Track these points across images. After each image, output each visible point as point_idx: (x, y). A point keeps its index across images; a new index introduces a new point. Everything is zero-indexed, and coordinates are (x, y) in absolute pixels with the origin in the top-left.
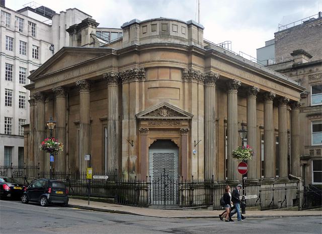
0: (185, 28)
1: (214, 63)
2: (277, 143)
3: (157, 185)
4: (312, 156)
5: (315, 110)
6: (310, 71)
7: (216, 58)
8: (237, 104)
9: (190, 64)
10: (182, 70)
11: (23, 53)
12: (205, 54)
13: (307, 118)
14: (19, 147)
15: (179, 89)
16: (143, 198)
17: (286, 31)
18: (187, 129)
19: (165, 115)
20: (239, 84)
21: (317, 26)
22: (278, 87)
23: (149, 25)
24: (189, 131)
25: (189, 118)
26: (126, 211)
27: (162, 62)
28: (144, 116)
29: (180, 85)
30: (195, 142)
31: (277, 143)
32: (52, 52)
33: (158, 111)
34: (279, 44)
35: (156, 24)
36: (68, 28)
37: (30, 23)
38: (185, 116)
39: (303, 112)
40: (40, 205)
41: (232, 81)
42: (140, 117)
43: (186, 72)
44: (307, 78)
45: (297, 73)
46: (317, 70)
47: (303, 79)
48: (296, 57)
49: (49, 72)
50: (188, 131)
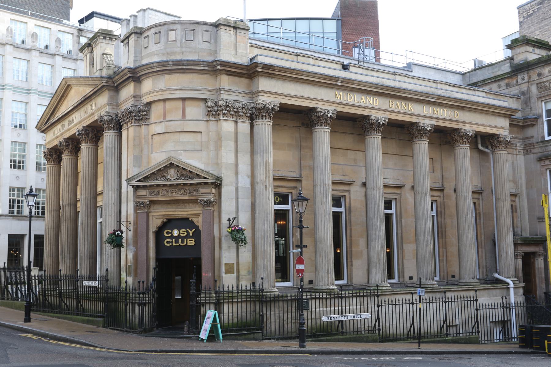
1: (264, 84)
6: (539, 75)
7: (271, 76)
8: (381, 152)
12: (248, 70)
13: (538, 165)
14: (9, 235)
16: (310, 321)
23: (151, 33)
24: (218, 201)
27: (168, 92)
28: (139, 181)
33: (161, 172)
38: (205, 178)
39: (531, 153)
40: (480, 344)
44: (534, 89)
45: (517, 82)
47: (529, 90)
48: (518, 50)
49: (59, 115)
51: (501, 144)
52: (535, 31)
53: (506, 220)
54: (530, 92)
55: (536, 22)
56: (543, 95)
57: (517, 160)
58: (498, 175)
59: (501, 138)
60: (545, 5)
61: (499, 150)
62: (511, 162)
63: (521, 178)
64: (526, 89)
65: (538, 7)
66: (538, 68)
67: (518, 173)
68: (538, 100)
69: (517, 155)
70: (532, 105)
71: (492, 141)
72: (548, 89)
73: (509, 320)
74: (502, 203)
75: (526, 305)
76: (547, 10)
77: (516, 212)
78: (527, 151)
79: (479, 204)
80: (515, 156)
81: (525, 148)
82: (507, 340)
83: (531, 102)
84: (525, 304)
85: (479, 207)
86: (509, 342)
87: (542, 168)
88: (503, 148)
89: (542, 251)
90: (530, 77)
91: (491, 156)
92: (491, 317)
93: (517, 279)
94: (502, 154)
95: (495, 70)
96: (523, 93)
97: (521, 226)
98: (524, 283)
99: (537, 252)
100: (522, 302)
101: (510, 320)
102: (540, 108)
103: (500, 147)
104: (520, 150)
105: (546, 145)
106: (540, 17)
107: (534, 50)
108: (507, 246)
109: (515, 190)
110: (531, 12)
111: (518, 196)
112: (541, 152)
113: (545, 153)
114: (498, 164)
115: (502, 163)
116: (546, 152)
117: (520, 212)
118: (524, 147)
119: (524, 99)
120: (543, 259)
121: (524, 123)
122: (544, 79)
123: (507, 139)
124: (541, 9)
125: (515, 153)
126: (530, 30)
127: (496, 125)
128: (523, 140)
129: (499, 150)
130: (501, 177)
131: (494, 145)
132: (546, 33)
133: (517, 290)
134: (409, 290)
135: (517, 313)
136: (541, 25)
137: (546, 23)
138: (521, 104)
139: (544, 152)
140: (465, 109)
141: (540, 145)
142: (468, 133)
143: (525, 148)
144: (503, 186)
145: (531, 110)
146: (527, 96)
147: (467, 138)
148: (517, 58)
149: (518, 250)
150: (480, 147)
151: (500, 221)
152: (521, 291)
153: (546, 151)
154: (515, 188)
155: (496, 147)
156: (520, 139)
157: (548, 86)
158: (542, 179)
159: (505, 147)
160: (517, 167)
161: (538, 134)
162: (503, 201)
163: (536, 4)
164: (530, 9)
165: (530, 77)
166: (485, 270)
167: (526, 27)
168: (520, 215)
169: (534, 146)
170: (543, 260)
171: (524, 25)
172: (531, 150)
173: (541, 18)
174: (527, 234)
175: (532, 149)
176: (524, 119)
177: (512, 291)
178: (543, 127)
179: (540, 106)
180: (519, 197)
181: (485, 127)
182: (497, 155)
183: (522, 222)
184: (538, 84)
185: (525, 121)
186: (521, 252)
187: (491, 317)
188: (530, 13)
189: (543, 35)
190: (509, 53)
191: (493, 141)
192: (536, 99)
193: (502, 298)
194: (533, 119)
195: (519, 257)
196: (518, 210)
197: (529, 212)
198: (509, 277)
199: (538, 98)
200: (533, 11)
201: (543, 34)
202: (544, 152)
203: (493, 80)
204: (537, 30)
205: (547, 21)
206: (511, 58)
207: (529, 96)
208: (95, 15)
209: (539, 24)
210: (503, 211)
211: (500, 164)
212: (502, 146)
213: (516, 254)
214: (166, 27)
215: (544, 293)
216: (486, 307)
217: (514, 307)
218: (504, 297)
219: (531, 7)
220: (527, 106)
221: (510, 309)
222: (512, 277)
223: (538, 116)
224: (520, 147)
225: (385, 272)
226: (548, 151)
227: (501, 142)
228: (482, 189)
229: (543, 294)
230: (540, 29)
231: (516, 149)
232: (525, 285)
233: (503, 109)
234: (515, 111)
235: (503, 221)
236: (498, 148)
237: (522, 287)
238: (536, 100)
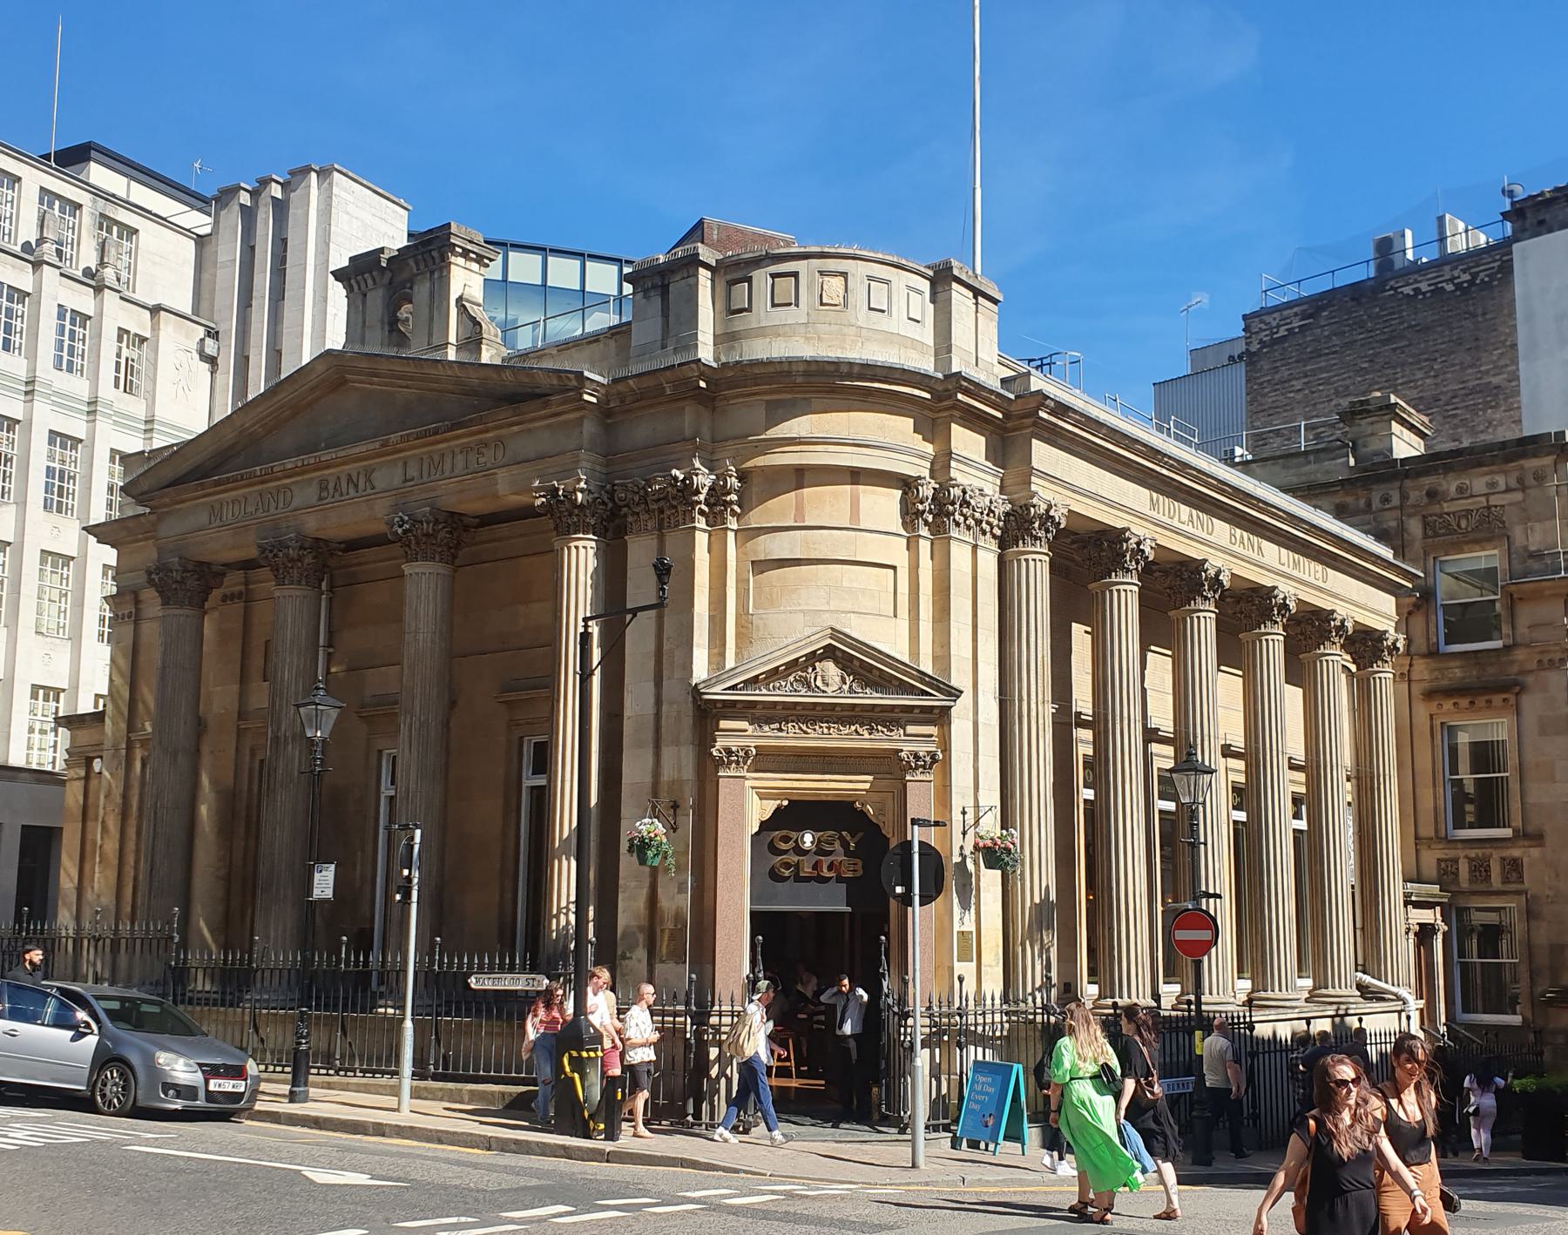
0: (920, 292)
1: (1043, 454)
2: (1241, 816)
3: (989, 1020)
7: (1055, 437)
9: (942, 463)
10: (907, 484)
11: (70, 363)
14: (23, 826)
15: (894, 568)
18: (933, 756)
19: (831, 681)
20: (1147, 550)
21: (1438, 291)
22: (1312, 570)
25: (938, 700)
28: (733, 687)
29: (896, 552)
30: (964, 813)
31: (1241, 816)
32: (207, 366)
34: (1265, 365)
36: (340, 261)
37: (105, 222)
41: (1118, 535)
42: (717, 692)
43: (927, 491)
45: (1369, 504)
50: (934, 760)
52: (1290, 380)
54: (1405, 535)
55: (1294, 359)
64: (1393, 524)
76: (1326, 333)
90: (1404, 497)
94: (1039, 563)
106: (1306, 348)
110: (1282, 332)
126: (1277, 377)
132: (1321, 388)
134: (1321, 1008)
136: (1308, 368)
137: (1323, 364)
164: (1278, 326)
165: (1404, 497)
167: (1266, 367)
171: (1262, 363)
173: (1309, 350)
189: (1313, 392)
200: (1287, 330)
201: (1314, 390)
204: (1296, 379)
205: (1325, 361)
208: (93, 154)
209: (1305, 366)
214: (816, 263)
225: (129, 909)
230: (1306, 376)
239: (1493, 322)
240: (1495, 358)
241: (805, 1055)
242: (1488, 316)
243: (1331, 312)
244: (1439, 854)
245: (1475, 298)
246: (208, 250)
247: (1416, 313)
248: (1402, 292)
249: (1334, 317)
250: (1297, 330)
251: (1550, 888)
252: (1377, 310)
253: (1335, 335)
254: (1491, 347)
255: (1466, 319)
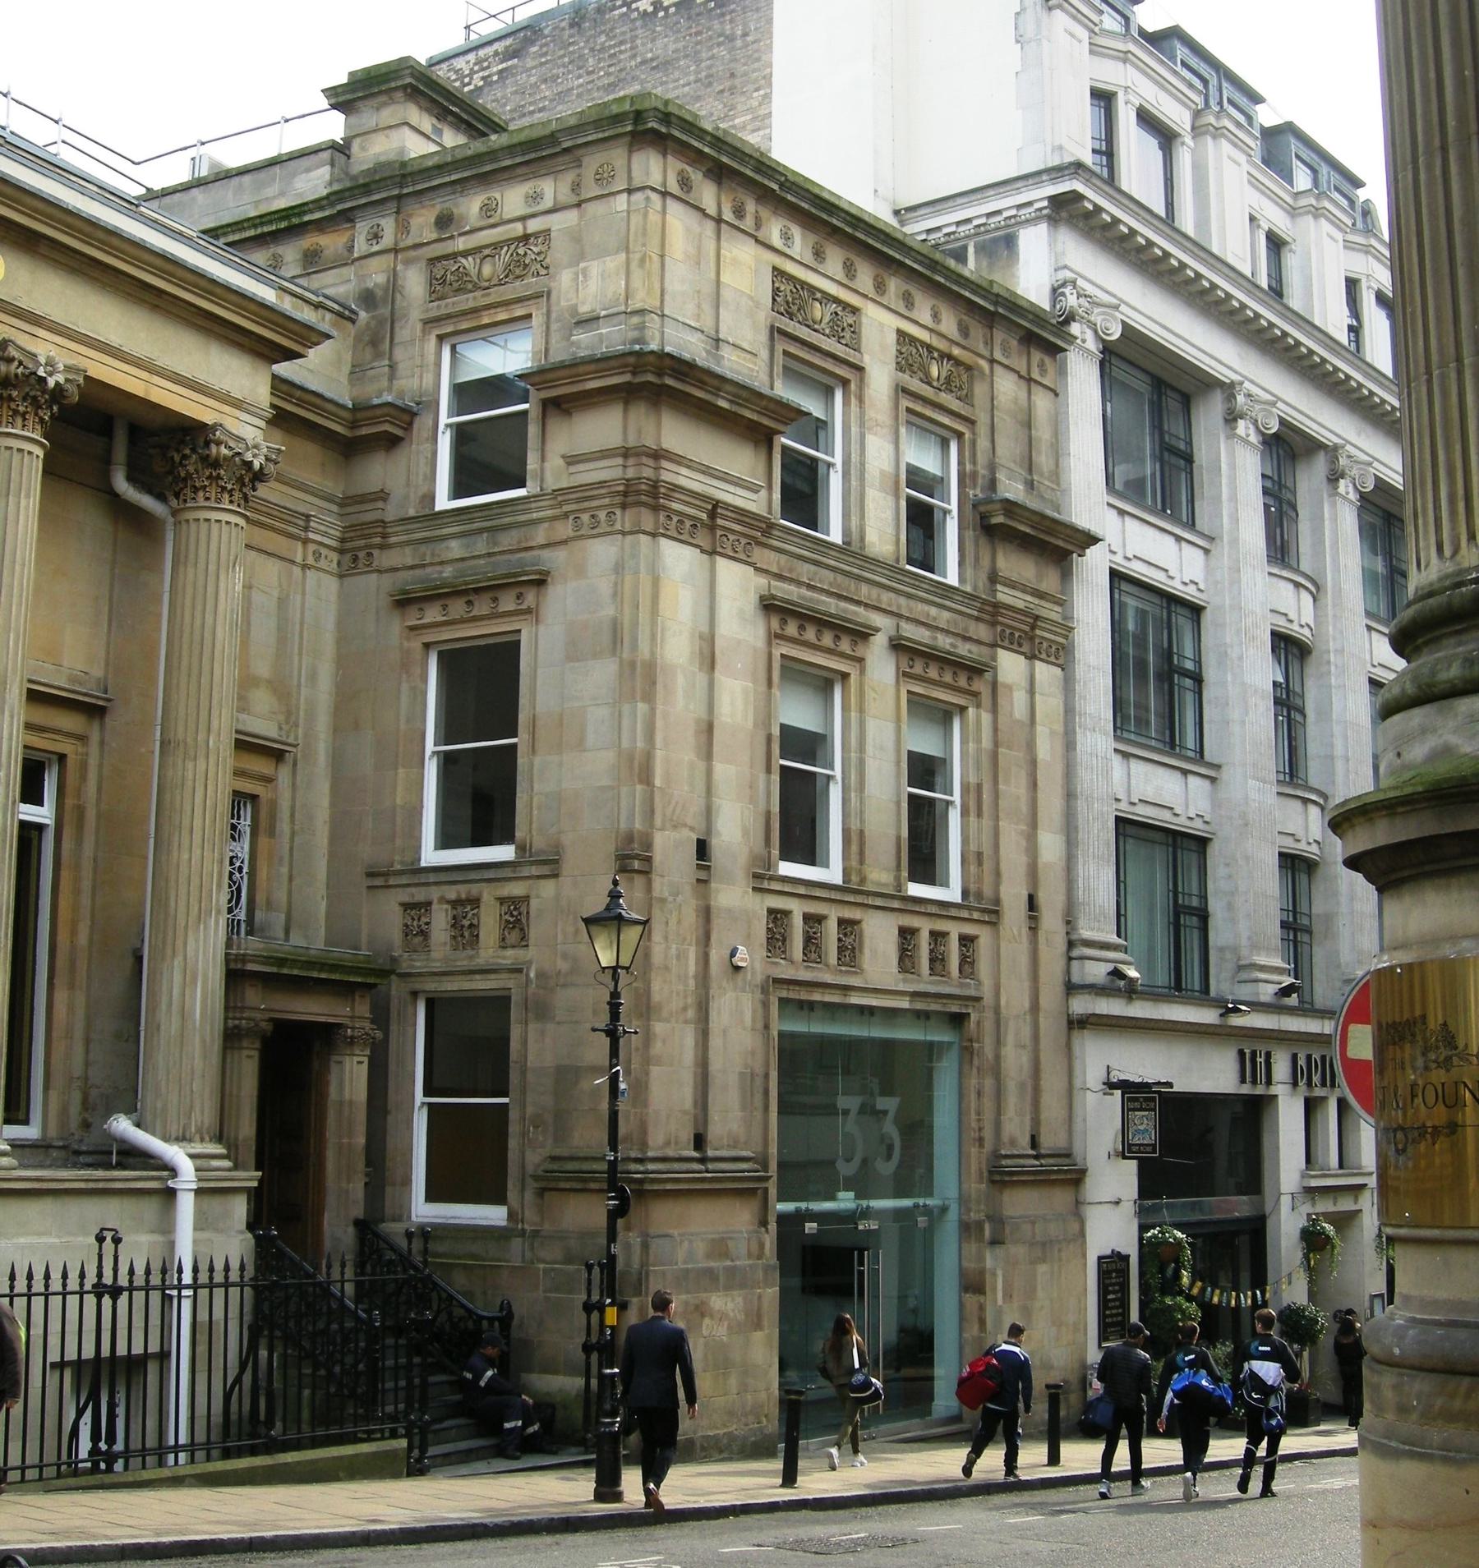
4: (419, 965)
5: (455, 548)
13: (396, 626)
17: (499, 46)
26: (61, 895)
35: (529, 316)
44: (414, 283)
46: (488, 209)
47: (393, 286)
48: (368, 118)
51: (219, 477)
53: (197, 852)
54: (398, 296)
56: (450, 310)
57: (304, 594)
58: (187, 629)
59: (218, 443)
60: (530, 63)
61: (207, 504)
62: (276, 593)
63: (313, 677)
65: (504, 65)
66: (441, 192)
67: (300, 654)
68: (423, 331)
69: (305, 567)
70: (399, 354)
71: (177, 458)
72: (470, 286)
73: (154, 1355)
74: (190, 765)
75: (356, 1274)
76: (533, 79)
77: (272, 832)
78: (355, 559)
79: (84, 766)
80: (297, 571)
81: (348, 545)
82: (103, 1466)
83: (396, 340)
84: (250, 1272)
85: (83, 777)
86: (108, 1479)
87: (408, 639)
88: (226, 496)
89: (367, 1025)
91: (170, 536)
92: (54, 1341)
93: (224, 1151)
94: (215, 527)
95: (270, 192)
96: (368, 298)
97: (289, 903)
98: (257, 1169)
99: (339, 1026)
100: (235, 1265)
101: (163, 1356)
102: (432, 367)
103: (213, 492)
104: (324, 551)
105: (438, 533)
106: (505, 105)
107: (439, 132)
108: (189, 979)
109: (280, 729)
111: (289, 758)
112: (412, 567)
113: (429, 570)
114: (191, 571)
115: (212, 568)
116: (432, 564)
117: (293, 834)
118: (343, 540)
119: (368, 323)
120: (366, 1060)
121: (354, 425)
122: (462, 239)
123: (248, 457)
124: (513, 75)
125: (299, 559)
127: (202, 376)
128: (341, 505)
129: (207, 504)
130: (197, 638)
131: (185, 480)
133: (215, 1204)
135: (203, 1316)
138: (355, 346)
139: (424, 566)
140: (43, 250)
141: (412, 531)
142: (41, 372)
143: (348, 545)
144: (205, 680)
145: (392, 377)
146: (385, 311)
147: (35, 398)
148: (363, 149)
149: (243, 1008)
150: (122, 485)
151: (169, 852)
152: (240, 1208)
153: (437, 560)
154: (282, 718)
155: (196, 490)
156: (329, 498)
157: (473, 272)
158: (405, 687)
159: (237, 495)
160: (302, 624)
161: (408, 485)
162: (195, 759)
163: (496, 53)
164: (472, 72)
166: (76, 1097)
168: (291, 849)
169: (384, 536)
170: (365, 1066)
172: (370, 555)
174: (312, 939)
175: (376, 552)
176: (356, 408)
177: (186, 1204)
178: (435, 453)
179: (431, 358)
180: (295, 764)
181: (144, 375)
182: (193, 526)
183: (296, 882)
184: (433, 261)
185: (359, 415)
186: (258, 1016)
187: (54, 1341)
188: (472, 87)
190: (334, 127)
191: (185, 457)
192: (419, 326)
193: (100, 1239)
194: (392, 411)
195: (245, 1044)
196: (284, 826)
197: (334, 839)
198: (181, 1139)
199: (429, 323)
200: (483, 78)
202: (424, 566)
203: (251, 233)
206: (341, 149)
207: (392, 313)
210: (187, 808)
211: (201, 578)
212: (224, 489)
213: (231, 1023)
215: (358, 1223)
216: (29, 1287)
217: (187, 1287)
218: (109, 1236)
219: (479, 62)
220: (378, 355)
221: (166, 1299)
222: (197, 1137)
223: (418, 404)
224: (325, 534)
226: (442, 563)
227: (216, 464)
228: (106, 692)
229: (351, 1230)
231: (306, 541)
232: (261, 1181)
233: (245, 303)
234: (304, 332)
235: (186, 856)
236: (201, 494)
237: (247, 1190)
238: (419, 333)
239: (755, 46)
240: (755, 103)
241: (482, 1384)
242: (749, 39)
243: (541, 47)
244: (405, 896)
245: (733, 11)
246: (1193, 845)
247: (653, 40)
248: (637, 9)
249: (546, 54)
250: (495, 78)
251: (565, 956)
252: (603, 38)
253: (545, 81)
254: (751, 87)
255: (719, 45)
